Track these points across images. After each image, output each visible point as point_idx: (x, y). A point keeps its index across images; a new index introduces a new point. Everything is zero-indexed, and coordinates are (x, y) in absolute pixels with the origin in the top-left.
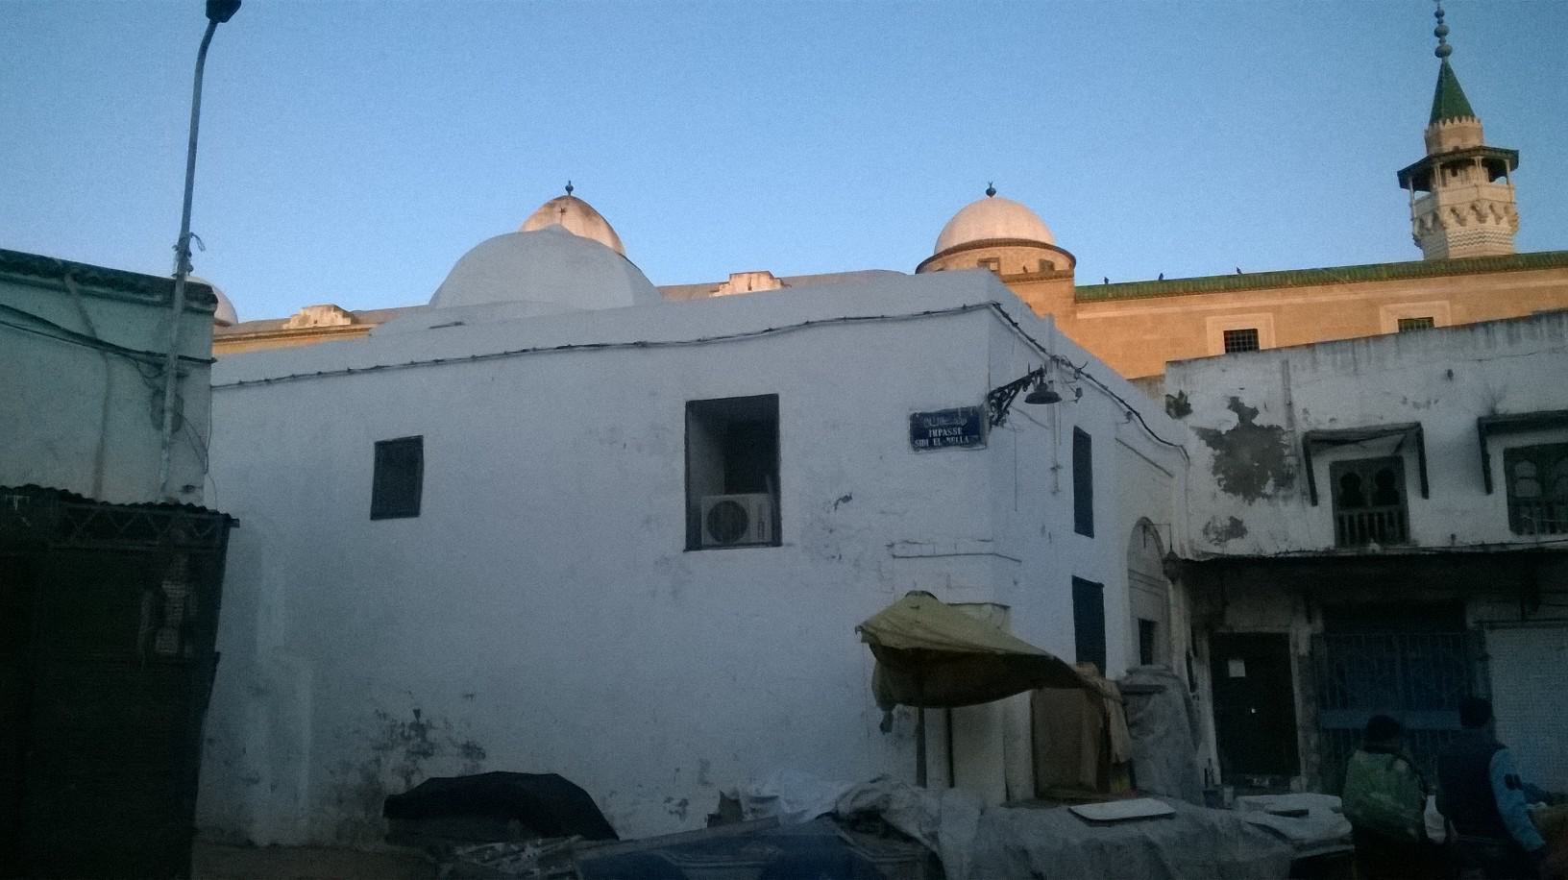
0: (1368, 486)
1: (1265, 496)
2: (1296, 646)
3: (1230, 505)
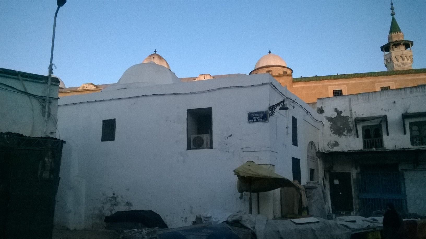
0: (372, 133)
1: (344, 135)
2: (352, 176)
3: (335, 138)
